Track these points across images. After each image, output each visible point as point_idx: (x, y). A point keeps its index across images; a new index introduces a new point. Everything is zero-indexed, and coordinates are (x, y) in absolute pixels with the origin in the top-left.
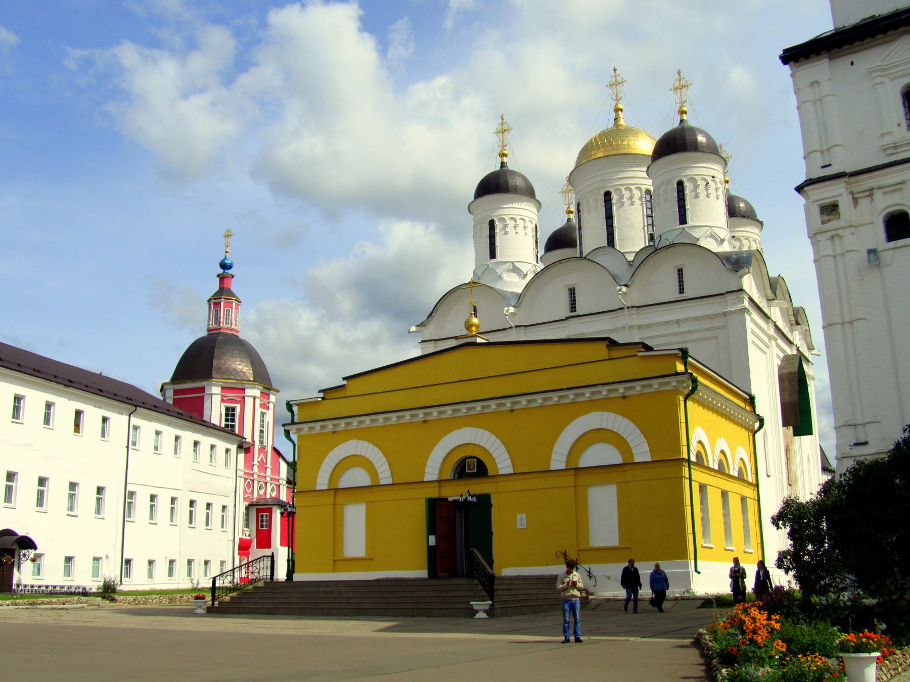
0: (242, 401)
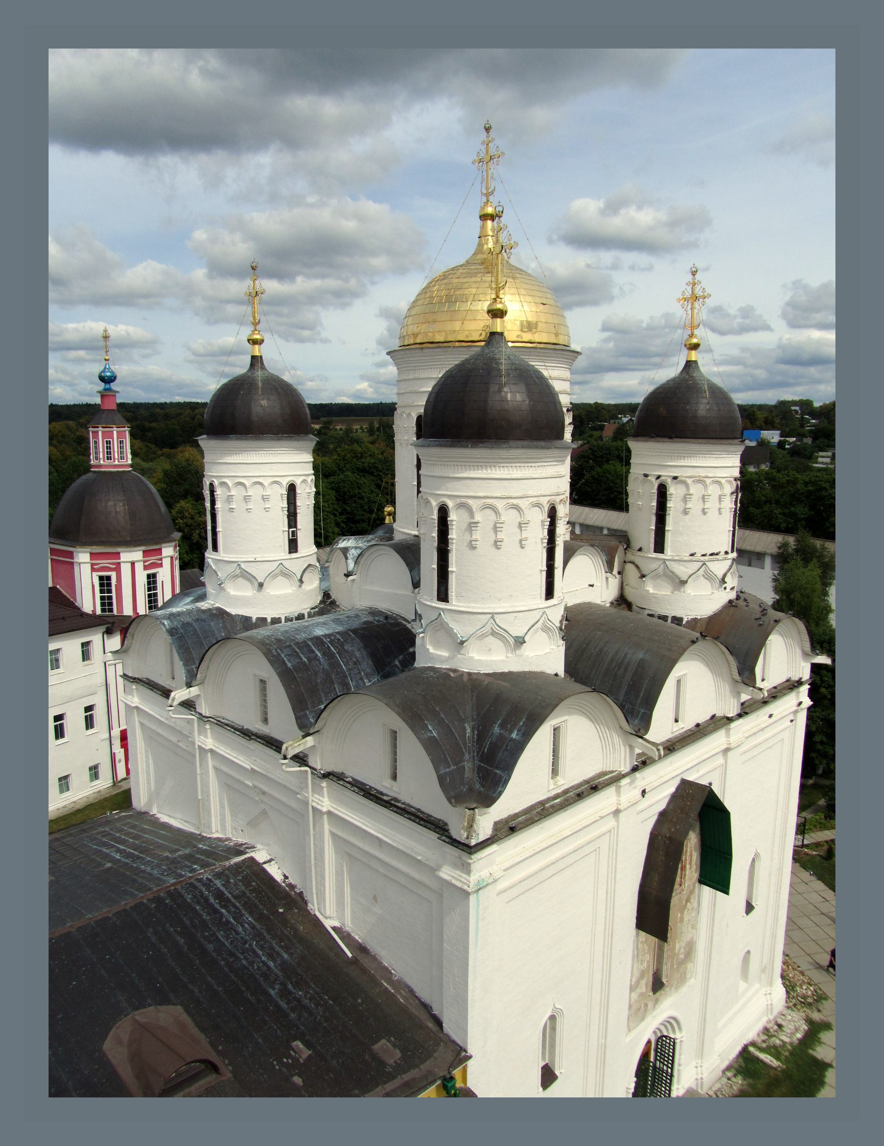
0: (118, 569)
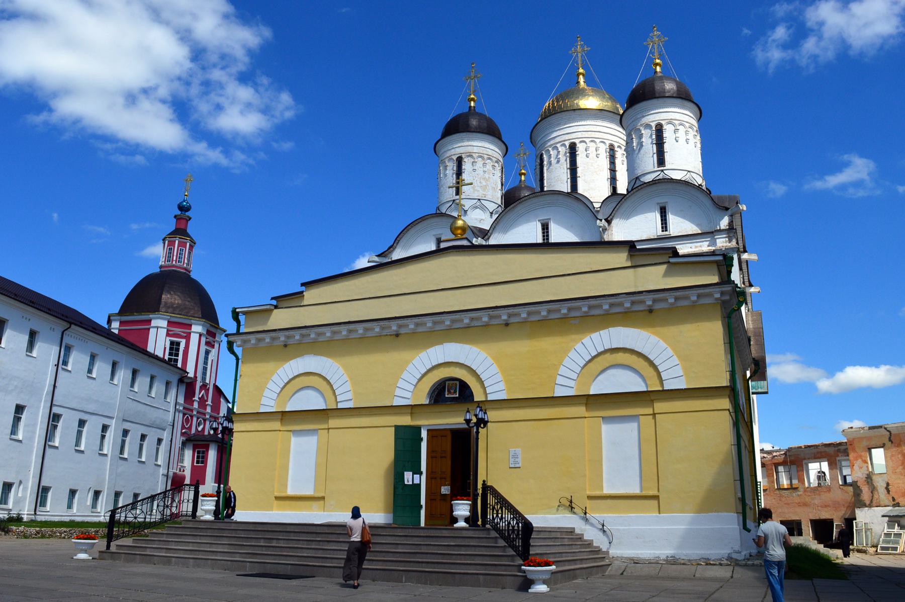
0: (188, 338)
